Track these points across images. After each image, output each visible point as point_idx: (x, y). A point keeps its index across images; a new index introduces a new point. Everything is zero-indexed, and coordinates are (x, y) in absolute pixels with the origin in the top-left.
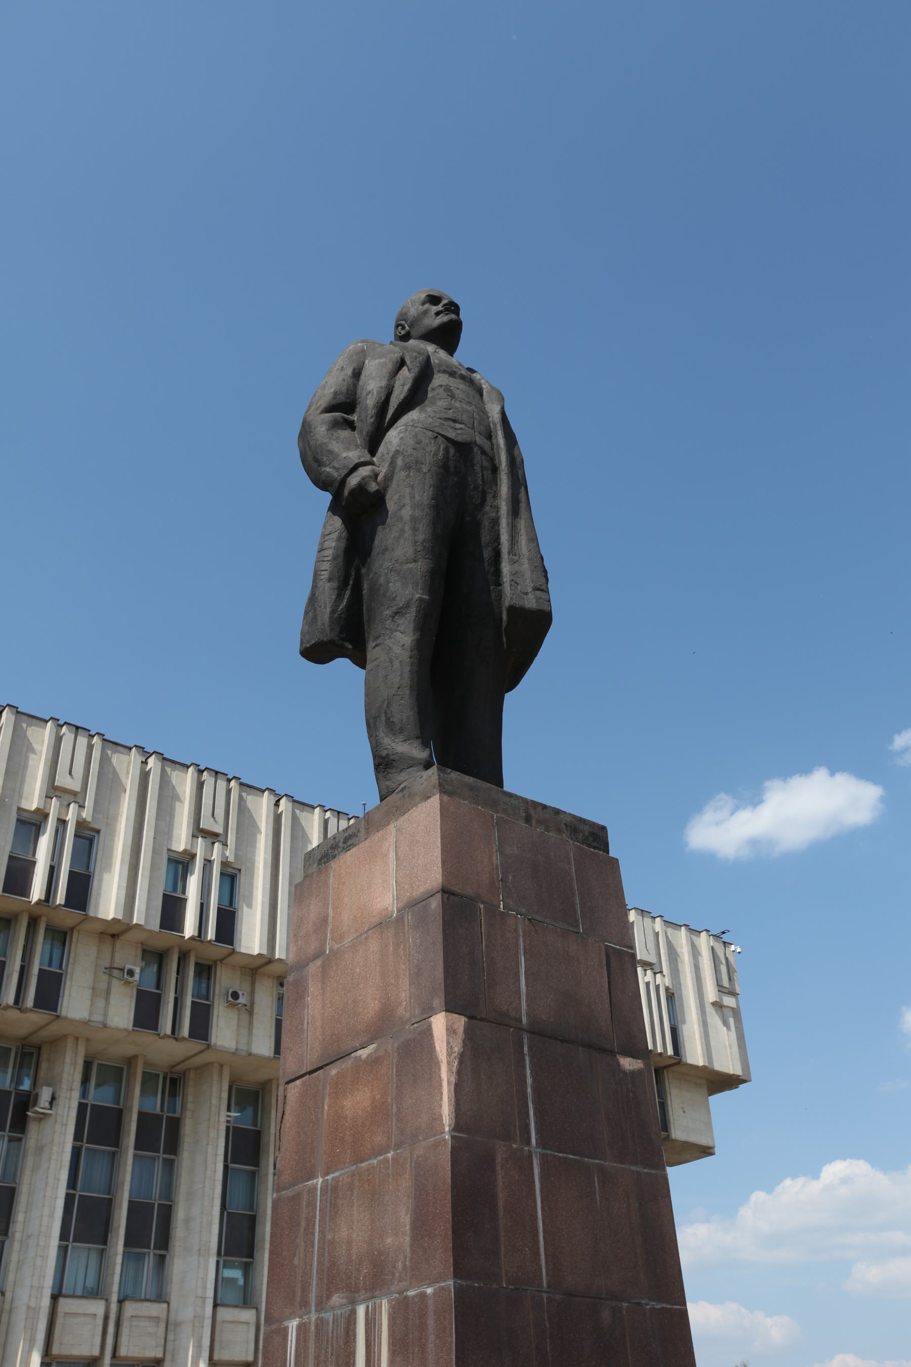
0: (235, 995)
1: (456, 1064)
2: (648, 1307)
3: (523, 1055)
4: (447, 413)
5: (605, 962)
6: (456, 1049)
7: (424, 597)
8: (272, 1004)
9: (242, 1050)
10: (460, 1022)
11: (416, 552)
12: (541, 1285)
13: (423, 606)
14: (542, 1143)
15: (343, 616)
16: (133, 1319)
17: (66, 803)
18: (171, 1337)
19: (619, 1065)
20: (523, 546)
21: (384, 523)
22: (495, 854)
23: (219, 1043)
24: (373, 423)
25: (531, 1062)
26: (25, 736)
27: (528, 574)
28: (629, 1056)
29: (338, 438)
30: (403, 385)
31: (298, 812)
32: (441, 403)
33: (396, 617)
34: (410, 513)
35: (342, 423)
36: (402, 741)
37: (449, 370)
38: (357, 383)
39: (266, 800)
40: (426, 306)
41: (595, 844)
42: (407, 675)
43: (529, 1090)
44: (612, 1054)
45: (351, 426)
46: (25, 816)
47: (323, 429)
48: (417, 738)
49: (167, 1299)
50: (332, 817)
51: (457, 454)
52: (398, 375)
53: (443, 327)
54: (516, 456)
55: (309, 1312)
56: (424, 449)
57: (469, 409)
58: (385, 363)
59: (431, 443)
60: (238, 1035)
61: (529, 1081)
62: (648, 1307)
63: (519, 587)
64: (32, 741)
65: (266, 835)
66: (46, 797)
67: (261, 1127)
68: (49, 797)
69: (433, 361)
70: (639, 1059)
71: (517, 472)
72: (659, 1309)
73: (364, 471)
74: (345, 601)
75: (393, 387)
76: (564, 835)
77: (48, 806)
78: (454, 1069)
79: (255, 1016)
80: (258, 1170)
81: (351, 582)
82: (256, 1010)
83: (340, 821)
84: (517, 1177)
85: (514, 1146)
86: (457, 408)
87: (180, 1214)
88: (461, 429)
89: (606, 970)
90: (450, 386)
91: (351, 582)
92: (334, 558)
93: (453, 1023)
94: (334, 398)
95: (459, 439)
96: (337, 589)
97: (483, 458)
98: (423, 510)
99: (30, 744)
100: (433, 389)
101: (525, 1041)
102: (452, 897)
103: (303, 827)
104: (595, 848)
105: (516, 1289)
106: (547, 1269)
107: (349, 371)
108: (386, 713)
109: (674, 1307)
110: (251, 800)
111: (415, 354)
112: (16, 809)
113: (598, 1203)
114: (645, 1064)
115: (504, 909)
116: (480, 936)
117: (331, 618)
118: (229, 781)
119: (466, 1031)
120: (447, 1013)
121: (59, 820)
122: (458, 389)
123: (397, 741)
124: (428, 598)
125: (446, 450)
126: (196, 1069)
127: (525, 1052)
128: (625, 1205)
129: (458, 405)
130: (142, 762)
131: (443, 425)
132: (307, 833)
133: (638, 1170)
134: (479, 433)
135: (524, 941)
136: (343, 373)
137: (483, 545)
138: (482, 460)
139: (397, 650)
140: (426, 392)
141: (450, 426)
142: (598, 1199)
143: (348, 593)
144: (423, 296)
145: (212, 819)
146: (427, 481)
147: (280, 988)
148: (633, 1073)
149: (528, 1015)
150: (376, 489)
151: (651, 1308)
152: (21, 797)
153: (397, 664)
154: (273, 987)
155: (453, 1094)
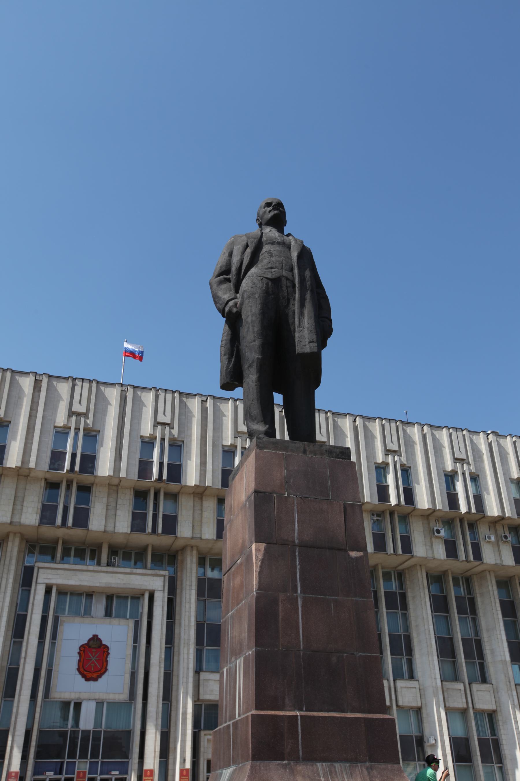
1: (260, 563)
2: (358, 655)
3: (295, 556)
4: (267, 265)
5: (343, 511)
6: (260, 557)
7: (259, 357)
8: (369, 525)
10: (262, 546)
11: (254, 336)
13: (259, 361)
14: (303, 591)
15: (232, 370)
17: (245, 439)
19: (349, 555)
20: (305, 322)
21: (242, 326)
22: (284, 471)
24: (235, 279)
25: (299, 559)
26: (220, 409)
27: (306, 336)
28: (355, 551)
29: (221, 289)
30: (247, 257)
31: (367, 423)
32: (265, 261)
33: (250, 368)
34: (251, 319)
35: (224, 281)
36: (256, 424)
37: (271, 242)
38: (231, 259)
39: (348, 421)
40: (265, 209)
41: (343, 457)
42: (255, 394)
43: (298, 570)
44: (346, 550)
45: (229, 280)
46: (226, 449)
47: (215, 286)
48: (262, 421)
50: (386, 423)
51: (273, 285)
52: (246, 252)
53: (274, 216)
54: (306, 275)
55: (228, 665)
56: (257, 287)
57: (280, 259)
58: (240, 248)
59: (259, 282)
61: (298, 567)
62: (358, 655)
63: (302, 343)
64: (223, 411)
65: (351, 438)
66: (234, 437)
67: (376, 589)
68: (235, 437)
69: (264, 239)
70: (361, 551)
71: (306, 284)
72: (364, 656)
73: (231, 303)
74: (232, 363)
75: (243, 258)
76: (325, 456)
77: (236, 442)
78: (259, 566)
80: (378, 611)
81: (235, 354)
83: (391, 424)
84: (289, 607)
85: (289, 594)
86: (273, 261)
88: (275, 271)
89: (343, 514)
90: (271, 250)
91: (235, 354)
92: (226, 345)
93: (259, 547)
94: (220, 269)
95: (273, 277)
96: (228, 358)
97: (287, 282)
98: (256, 317)
99: (223, 412)
100: (262, 255)
101: (297, 550)
102: (260, 494)
103: (371, 431)
104: (342, 459)
105: (287, 650)
106: (303, 642)
107: (227, 254)
108: (249, 412)
109: (373, 655)
110: (340, 421)
111: (252, 240)
112: (221, 446)
113: (333, 614)
114: (364, 553)
115: (287, 495)
116: (274, 509)
117: (226, 372)
118: (326, 413)
119: (265, 549)
120: (256, 543)
121: (242, 448)
122: (275, 250)
123: (254, 424)
124: (261, 357)
125: (267, 284)
127: (296, 555)
128: (348, 615)
129: (274, 259)
130: (279, 411)
131: (265, 272)
132: (374, 433)
133: (357, 599)
134: (286, 270)
135: (297, 507)
136: (225, 255)
137: (290, 324)
138: (287, 283)
139: (251, 383)
140: (259, 257)
141: (268, 272)
142: (333, 612)
143: (233, 359)
144: (264, 204)
145: (320, 435)
146: (258, 302)
147: (372, 516)
148: (357, 558)
149: (299, 539)
150: (236, 310)
151: (359, 656)
152: (222, 439)
153: (251, 389)
154: (368, 517)
155: (258, 576)
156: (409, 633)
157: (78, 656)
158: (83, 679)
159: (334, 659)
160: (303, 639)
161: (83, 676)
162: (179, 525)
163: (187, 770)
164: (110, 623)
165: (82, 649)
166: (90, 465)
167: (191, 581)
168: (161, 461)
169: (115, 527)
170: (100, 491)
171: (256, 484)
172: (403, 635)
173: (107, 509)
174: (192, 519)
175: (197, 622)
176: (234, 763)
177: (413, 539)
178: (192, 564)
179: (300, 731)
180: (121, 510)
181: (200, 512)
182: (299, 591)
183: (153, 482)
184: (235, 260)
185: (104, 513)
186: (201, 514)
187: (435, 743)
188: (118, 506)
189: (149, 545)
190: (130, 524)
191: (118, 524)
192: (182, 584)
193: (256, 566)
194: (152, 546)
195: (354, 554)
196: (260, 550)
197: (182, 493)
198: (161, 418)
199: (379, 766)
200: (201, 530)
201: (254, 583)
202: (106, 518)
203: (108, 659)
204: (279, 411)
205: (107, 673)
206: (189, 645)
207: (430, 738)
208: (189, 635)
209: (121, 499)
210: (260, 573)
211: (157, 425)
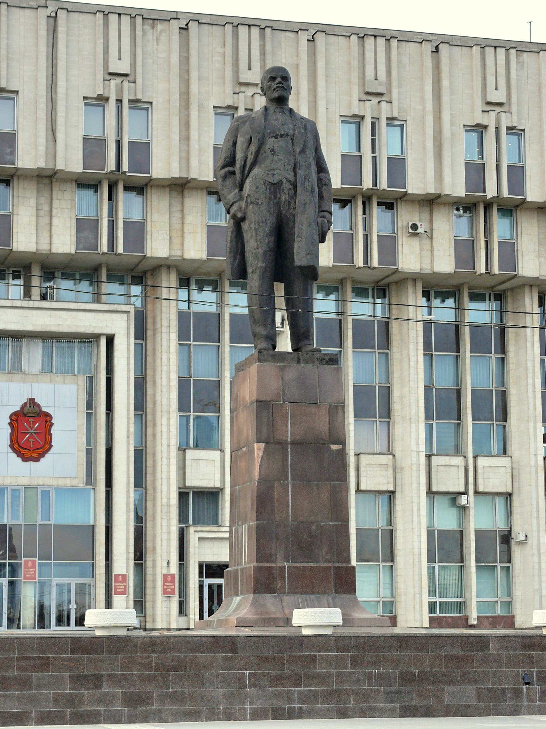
0: (415, 227)
1: (260, 459)
9: (426, 269)
12: (289, 521)
16: (368, 466)
18: (398, 477)
19: (330, 448)
23: (405, 267)
25: (291, 454)
43: (289, 463)
49: (393, 453)
60: (421, 257)
78: (259, 461)
79: (434, 240)
82: (435, 235)
87: (396, 394)
91: (239, 251)
94: (225, 161)
101: (289, 447)
107: (231, 143)
126: (397, 283)
131: (268, 174)
156: (506, 388)
157: (9, 427)
158: (20, 459)
159: (314, 527)
160: (291, 514)
161: (19, 454)
162: (149, 237)
163: (173, 576)
164: (51, 382)
165: (14, 418)
166: (9, 150)
167: (169, 320)
168: (119, 138)
169: (51, 244)
170: (24, 188)
171: (258, 395)
172: (495, 390)
173: (38, 216)
174: (168, 228)
175: (179, 377)
176: (242, 594)
177: (519, 248)
178: (170, 294)
179: (287, 575)
180: (59, 217)
181: (180, 216)
182: (290, 479)
183: (106, 173)
184: (239, 156)
185: (34, 223)
186: (183, 218)
187: (526, 540)
188: (54, 212)
189: (103, 265)
190: (74, 239)
191: (55, 240)
192: (154, 323)
193: (258, 462)
194: (108, 266)
195: (334, 447)
196: (260, 449)
197: (152, 186)
198: (116, 67)
199: (341, 596)
200: (183, 245)
201: (256, 474)
202: (37, 230)
203: (52, 432)
204: (308, 40)
205: (52, 451)
206: (169, 413)
207: (519, 533)
208: (169, 399)
209: (57, 199)
210: (260, 466)
211: (108, 77)
